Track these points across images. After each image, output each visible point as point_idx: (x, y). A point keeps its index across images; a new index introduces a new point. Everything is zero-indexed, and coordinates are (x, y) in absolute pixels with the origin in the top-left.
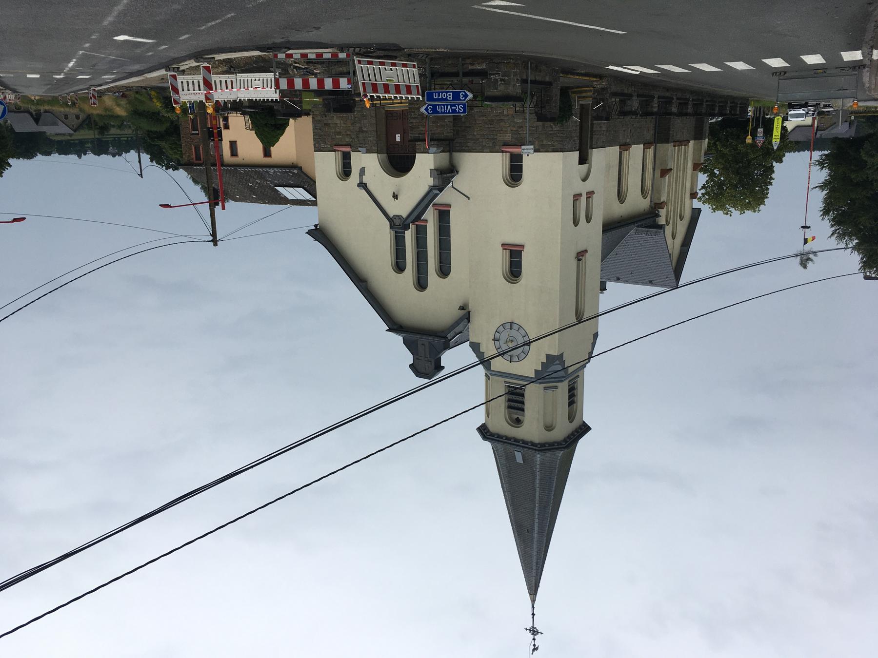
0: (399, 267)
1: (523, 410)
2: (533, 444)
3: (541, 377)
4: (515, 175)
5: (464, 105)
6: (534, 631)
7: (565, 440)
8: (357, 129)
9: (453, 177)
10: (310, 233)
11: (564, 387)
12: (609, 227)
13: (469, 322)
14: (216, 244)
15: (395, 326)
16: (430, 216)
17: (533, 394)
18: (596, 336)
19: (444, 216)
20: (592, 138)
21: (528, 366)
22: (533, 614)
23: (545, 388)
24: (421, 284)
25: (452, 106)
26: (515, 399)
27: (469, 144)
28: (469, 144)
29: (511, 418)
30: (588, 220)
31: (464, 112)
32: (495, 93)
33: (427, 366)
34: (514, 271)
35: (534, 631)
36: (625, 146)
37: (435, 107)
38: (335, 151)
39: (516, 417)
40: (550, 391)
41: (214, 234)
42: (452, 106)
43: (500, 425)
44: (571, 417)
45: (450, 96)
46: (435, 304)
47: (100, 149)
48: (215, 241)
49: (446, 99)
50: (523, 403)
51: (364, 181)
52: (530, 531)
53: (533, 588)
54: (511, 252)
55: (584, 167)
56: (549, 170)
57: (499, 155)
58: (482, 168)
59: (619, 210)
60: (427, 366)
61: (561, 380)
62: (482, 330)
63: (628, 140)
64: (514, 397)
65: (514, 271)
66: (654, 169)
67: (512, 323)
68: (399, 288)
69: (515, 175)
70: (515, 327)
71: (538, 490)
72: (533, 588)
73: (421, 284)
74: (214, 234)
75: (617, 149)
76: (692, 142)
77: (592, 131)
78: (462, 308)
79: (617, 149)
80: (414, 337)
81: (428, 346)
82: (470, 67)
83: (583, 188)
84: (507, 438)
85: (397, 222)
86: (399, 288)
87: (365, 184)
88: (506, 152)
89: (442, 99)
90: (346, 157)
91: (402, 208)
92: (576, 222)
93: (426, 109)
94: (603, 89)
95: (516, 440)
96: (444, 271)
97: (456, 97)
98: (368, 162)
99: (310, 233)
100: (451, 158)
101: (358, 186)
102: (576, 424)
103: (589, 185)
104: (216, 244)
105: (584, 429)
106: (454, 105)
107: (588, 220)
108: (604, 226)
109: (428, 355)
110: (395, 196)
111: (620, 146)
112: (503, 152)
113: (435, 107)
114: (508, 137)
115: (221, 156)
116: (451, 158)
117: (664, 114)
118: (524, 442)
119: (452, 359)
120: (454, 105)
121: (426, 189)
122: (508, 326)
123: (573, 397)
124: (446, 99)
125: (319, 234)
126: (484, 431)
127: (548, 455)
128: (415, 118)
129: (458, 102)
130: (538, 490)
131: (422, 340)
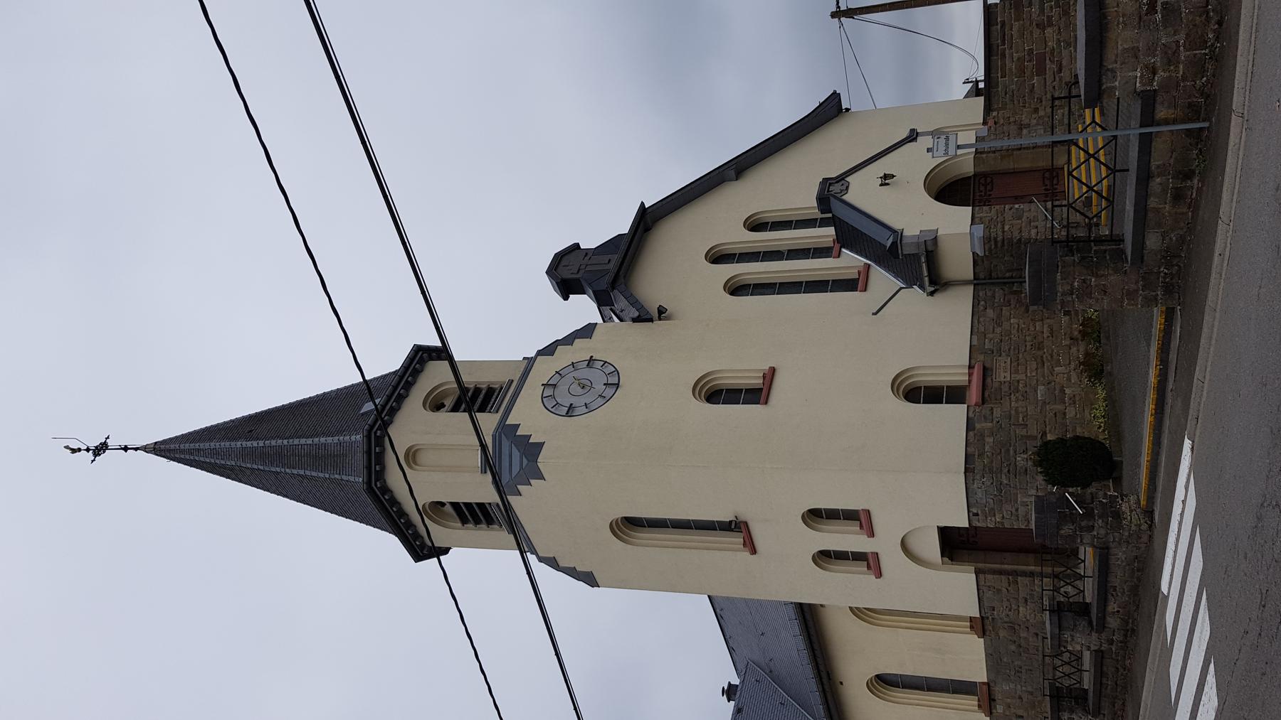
0: (755, 225)
3: (506, 431)
6: (100, 449)
8: (1026, 121)
9: (922, 287)
10: (835, 96)
11: (482, 491)
13: (635, 320)
14: (833, 15)
15: (647, 219)
16: (851, 261)
18: (590, 579)
19: (848, 285)
20: (1000, 572)
21: (529, 415)
22: (126, 449)
24: (718, 257)
26: (475, 398)
27: (990, 312)
28: (990, 312)
30: (825, 557)
33: (570, 272)
35: (100, 449)
36: (980, 626)
41: (850, 13)
46: (676, 269)
51: (919, 138)
52: (250, 436)
53: (164, 449)
55: (931, 547)
56: (923, 478)
58: (939, 333)
59: (855, 672)
60: (570, 272)
62: (621, 342)
63: (1000, 709)
67: (617, 385)
68: (722, 219)
69: (918, 393)
70: (610, 391)
71: (309, 441)
72: (164, 449)
73: (718, 257)
74: (850, 13)
77: (1015, 573)
78: (661, 311)
80: (623, 247)
83: (885, 544)
85: (836, 188)
87: (915, 139)
88: (970, 375)
90: (953, 394)
91: (863, 193)
92: (815, 516)
94: (1118, 515)
96: (737, 289)
99: (835, 96)
100: (966, 283)
101: (912, 131)
102: (439, 534)
103: (892, 559)
104: (833, 15)
105: (421, 549)
107: (825, 557)
109: (589, 268)
111: (988, 684)
112: (971, 367)
114: (1003, 374)
116: (966, 283)
122: (613, 380)
123: (473, 515)
127: (359, 459)
128: (1042, 10)
130: (309, 441)
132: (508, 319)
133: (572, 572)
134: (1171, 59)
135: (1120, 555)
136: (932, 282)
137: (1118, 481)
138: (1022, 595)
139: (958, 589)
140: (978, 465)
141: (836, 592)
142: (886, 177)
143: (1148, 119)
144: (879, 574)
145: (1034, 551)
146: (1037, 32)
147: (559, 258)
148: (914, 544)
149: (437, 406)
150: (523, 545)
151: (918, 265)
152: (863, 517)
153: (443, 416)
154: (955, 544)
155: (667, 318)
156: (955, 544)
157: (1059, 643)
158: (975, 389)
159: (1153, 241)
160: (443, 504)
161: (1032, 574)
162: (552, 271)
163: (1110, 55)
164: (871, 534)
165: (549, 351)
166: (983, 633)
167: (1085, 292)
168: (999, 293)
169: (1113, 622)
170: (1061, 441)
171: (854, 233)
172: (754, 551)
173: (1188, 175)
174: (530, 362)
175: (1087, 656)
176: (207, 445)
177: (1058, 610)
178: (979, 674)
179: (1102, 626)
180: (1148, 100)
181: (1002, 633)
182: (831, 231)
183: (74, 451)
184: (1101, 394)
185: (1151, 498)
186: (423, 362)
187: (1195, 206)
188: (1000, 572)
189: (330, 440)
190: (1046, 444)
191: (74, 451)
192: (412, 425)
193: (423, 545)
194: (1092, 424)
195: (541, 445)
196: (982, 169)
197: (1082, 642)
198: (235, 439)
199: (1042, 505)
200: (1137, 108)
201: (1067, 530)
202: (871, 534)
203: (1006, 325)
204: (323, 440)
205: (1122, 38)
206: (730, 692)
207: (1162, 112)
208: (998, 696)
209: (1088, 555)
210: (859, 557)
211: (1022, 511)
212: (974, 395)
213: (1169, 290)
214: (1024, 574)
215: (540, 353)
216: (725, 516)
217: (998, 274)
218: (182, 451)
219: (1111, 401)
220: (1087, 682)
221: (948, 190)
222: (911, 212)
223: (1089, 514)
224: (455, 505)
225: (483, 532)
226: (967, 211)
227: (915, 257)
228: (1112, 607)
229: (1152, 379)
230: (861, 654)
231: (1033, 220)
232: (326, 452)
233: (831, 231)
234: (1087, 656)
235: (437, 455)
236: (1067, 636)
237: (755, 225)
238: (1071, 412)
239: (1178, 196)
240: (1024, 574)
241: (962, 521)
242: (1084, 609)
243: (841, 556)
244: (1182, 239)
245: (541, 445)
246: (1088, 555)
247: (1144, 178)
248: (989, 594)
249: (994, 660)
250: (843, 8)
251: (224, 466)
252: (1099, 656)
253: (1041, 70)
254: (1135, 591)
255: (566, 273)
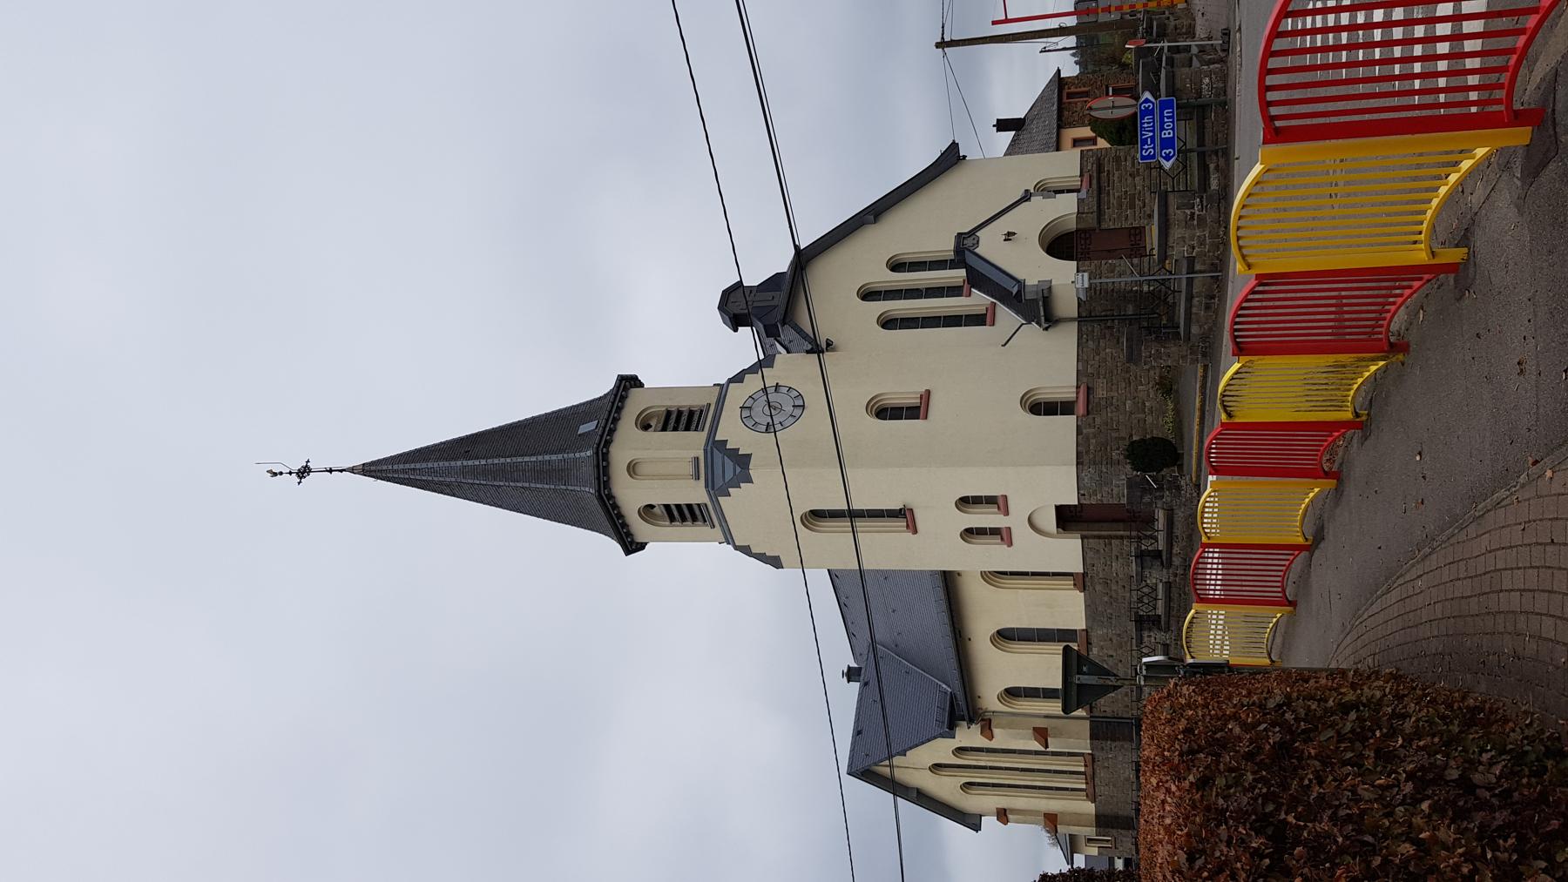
0: (896, 266)
1: (664, 429)
2: (608, 443)
3: (716, 447)
4: (1042, 408)
5: (1153, 157)
6: (304, 472)
7: (611, 497)
9: (1039, 323)
10: (954, 146)
11: (696, 494)
12: (948, 582)
14: (938, 45)
15: (804, 259)
16: (978, 300)
17: (692, 444)
18: (776, 562)
19: (978, 320)
20: (1099, 537)
21: (732, 431)
22: (331, 471)
23: (697, 459)
24: (868, 295)
25: (1153, 138)
26: (680, 419)
29: (650, 416)
30: (970, 533)
31: (1143, 158)
32: (1172, 208)
33: (739, 306)
34: (885, 412)
35: (304, 472)
36: (1082, 581)
37: (1151, 112)
38: (1081, 175)
39: (653, 423)
40: (690, 469)
41: (953, 43)
42: (1153, 138)
43: (635, 404)
44: (647, 511)
45: (1166, 134)
46: (834, 302)
47: (1078, 453)
48: (942, 44)
49: (1162, 128)
50: (675, 429)
52: (467, 455)
53: (373, 470)
54: (918, 408)
55: (1049, 521)
56: (1046, 473)
57: (1072, 380)
58: (1052, 359)
59: (981, 629)
60: (739, 306)
61: (710, 485)
62: (794, 369)
64: (684, 419)
65: (885, 412)
66: (1047, 717)
68: (866, 260)
69: (1042, 408)
70: (797, 412)
72: (373, 470)
73: (868, 295)
74: (953, 43)
75: (1078, 568)
76: (1089, 808)
77: (1110, 537)
78: (829, 344)
79: (1078, 568)
80: (786, 287)
81: (767, 309)
82: (1212, 166)
83: (1015, 521)
84: (619, 409)
85: (969, 242)
86: (866, 260)
89: (1162, 123)
90: (1064, 408)
91: (990, 246)
92: (965, 502)
93: (1147, 101)
94: (1179, 488)
95: (616, 420)
96: (888, 323)
97: (1167, 143)
98: (1066, 206)
99: (954, 146)
100: (1071, 320)
102: (640, 528)
103: (1021, 532)
104: (938, 45)
105: (631, 546)
106: (1153, 141)
107: (970, 533)
108: (950, 572)
110: (1009, 236)
112: (1078, 387)
113: (1151, 112)
114: (1101, 392)
115: (1072, 125)
116: (1071, 320)
117: (1133, 519)
118: (612, 431)
119: (743, 346)
120: (1153, 141)
121: (1020, 276)
123: (683, 515)
124: (1162, 128)
125: (951, 158)
126: (628, 383)
127: (588, 471)
129: (1158, 148)
130: (533, 459)
131: (780, 298)
132: (695, 352)
133: (762, 557)
134: (1202, 243)
135: (1180, 514)
136: (1047, 320)
137: (1181, 467)
138: (1115, 553)
139: (1068, 552)
140: (1085, 459)
141: (972, 560)
142: (1009, 234)
143: (1191, 270)
144: (1010, 544)
145: (1123, 521)
146: (1130, 180)
147: (727, 295)
148: (1038, 521)
149: (646, 427)
150: (728, 538)
151: (1036, 307)
152: (1001, 502)
153: (650, 434)
154: (1067, 518)
155: (834, 350)
156: (1067, 518)
157: (1142, 578)
158: (1085, 407)
159: (1195, 330)
160: (652, 507)
161: (1122, 537)
162: (722, 307)
163: (1171, 240)
164: (1007, 513)
165: (738, 378)
166: (1084, 589)
167: (1159, 355)
168: (1097, 328)
169: (1177, 561)
170: (1143, 441)
171: (982, 277)
172: (915, 531)
173: (1213, 297)
174: (722, 390)
175: (1160, 586)
176: (424, 465)
177: (1141, 556)
178: (1078, 621)
179: (1170, 564)
180: (1191, 261)
181: (1098, 588)
182: (962, 272)
183: (275, 474)
184: (1171, 406)
185: (1198, 477)
186: (625, 389)
187: (1216, 312)
188: (1099, 537)
189: (554, 457)
190: (1133, 443)
191: (275, 474)
192: (629, 444)
193: (632, 542)
194: (1164, 429)
195: (749, 456)
196: (1082, 226)
197: (1156, 577)
198: (455, 459)
199: (1131, 484)
200: (1185, 263)
201: (1147, 499)
202: (1007, 513)
203: (1103, 354)
204: (547, 457)
205: (1176, 233)
206: (851, 675)
207: (1198, 267)
208: (1094, 640)
209: (1160, 515)
210: (995, 532)
211: (1117, 490)
212: (1081, 408)
213: (1204, 355)
214: (1117, 537)
215: (731, 381)
216: (896, 506)
217: (1096, 316)
218: (396, 471)
219: (1178, 412)
220: (1160, 611)
221: (1058, 244)
222: (1032, 266)
223: (1161, 488)
224: (667, 507)
225: (688, 529)
226: (1072, 265)
227: (1035, 301)
228: (1176, 550)
229: (1198, 404)
230: (990, 610)
231: (1125, 275)
232: (554, 464)
233: (962, 272)
234: (1160, 586)
235: (653, 468)
236: (1147, 573)
237: (896, 266)
238: (1149, 419)
239: (1208, 307)
240: (1117, 537)
241: (1073, 500)
242: (1157, 555)
243: (981, 532)
244: (1210, 329)
245: (749, 456)
246: (1160, 515)
247: (1190, 298)
248: (1090, 554)
249: (1091, 610)
250: (947, 39)
251: (441, 483)
252: (1168, 586)
253: (1132, 206)
254: (1190, 537)
255: (739, 307)
